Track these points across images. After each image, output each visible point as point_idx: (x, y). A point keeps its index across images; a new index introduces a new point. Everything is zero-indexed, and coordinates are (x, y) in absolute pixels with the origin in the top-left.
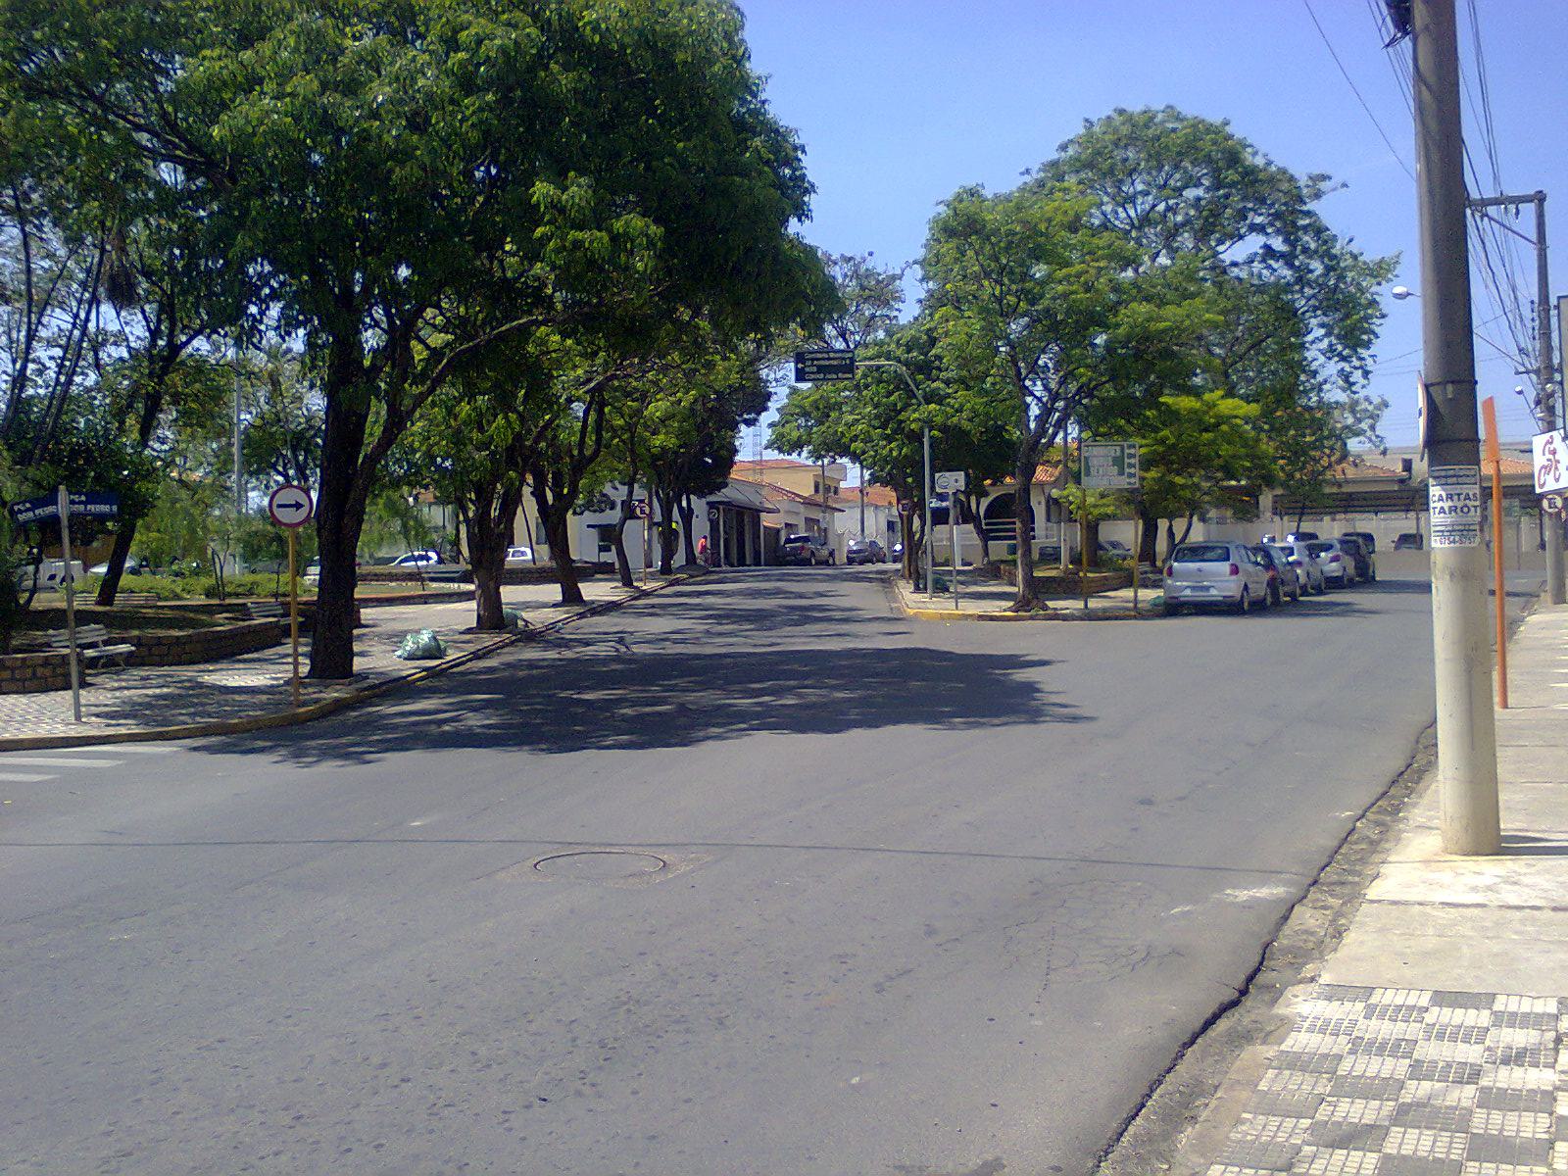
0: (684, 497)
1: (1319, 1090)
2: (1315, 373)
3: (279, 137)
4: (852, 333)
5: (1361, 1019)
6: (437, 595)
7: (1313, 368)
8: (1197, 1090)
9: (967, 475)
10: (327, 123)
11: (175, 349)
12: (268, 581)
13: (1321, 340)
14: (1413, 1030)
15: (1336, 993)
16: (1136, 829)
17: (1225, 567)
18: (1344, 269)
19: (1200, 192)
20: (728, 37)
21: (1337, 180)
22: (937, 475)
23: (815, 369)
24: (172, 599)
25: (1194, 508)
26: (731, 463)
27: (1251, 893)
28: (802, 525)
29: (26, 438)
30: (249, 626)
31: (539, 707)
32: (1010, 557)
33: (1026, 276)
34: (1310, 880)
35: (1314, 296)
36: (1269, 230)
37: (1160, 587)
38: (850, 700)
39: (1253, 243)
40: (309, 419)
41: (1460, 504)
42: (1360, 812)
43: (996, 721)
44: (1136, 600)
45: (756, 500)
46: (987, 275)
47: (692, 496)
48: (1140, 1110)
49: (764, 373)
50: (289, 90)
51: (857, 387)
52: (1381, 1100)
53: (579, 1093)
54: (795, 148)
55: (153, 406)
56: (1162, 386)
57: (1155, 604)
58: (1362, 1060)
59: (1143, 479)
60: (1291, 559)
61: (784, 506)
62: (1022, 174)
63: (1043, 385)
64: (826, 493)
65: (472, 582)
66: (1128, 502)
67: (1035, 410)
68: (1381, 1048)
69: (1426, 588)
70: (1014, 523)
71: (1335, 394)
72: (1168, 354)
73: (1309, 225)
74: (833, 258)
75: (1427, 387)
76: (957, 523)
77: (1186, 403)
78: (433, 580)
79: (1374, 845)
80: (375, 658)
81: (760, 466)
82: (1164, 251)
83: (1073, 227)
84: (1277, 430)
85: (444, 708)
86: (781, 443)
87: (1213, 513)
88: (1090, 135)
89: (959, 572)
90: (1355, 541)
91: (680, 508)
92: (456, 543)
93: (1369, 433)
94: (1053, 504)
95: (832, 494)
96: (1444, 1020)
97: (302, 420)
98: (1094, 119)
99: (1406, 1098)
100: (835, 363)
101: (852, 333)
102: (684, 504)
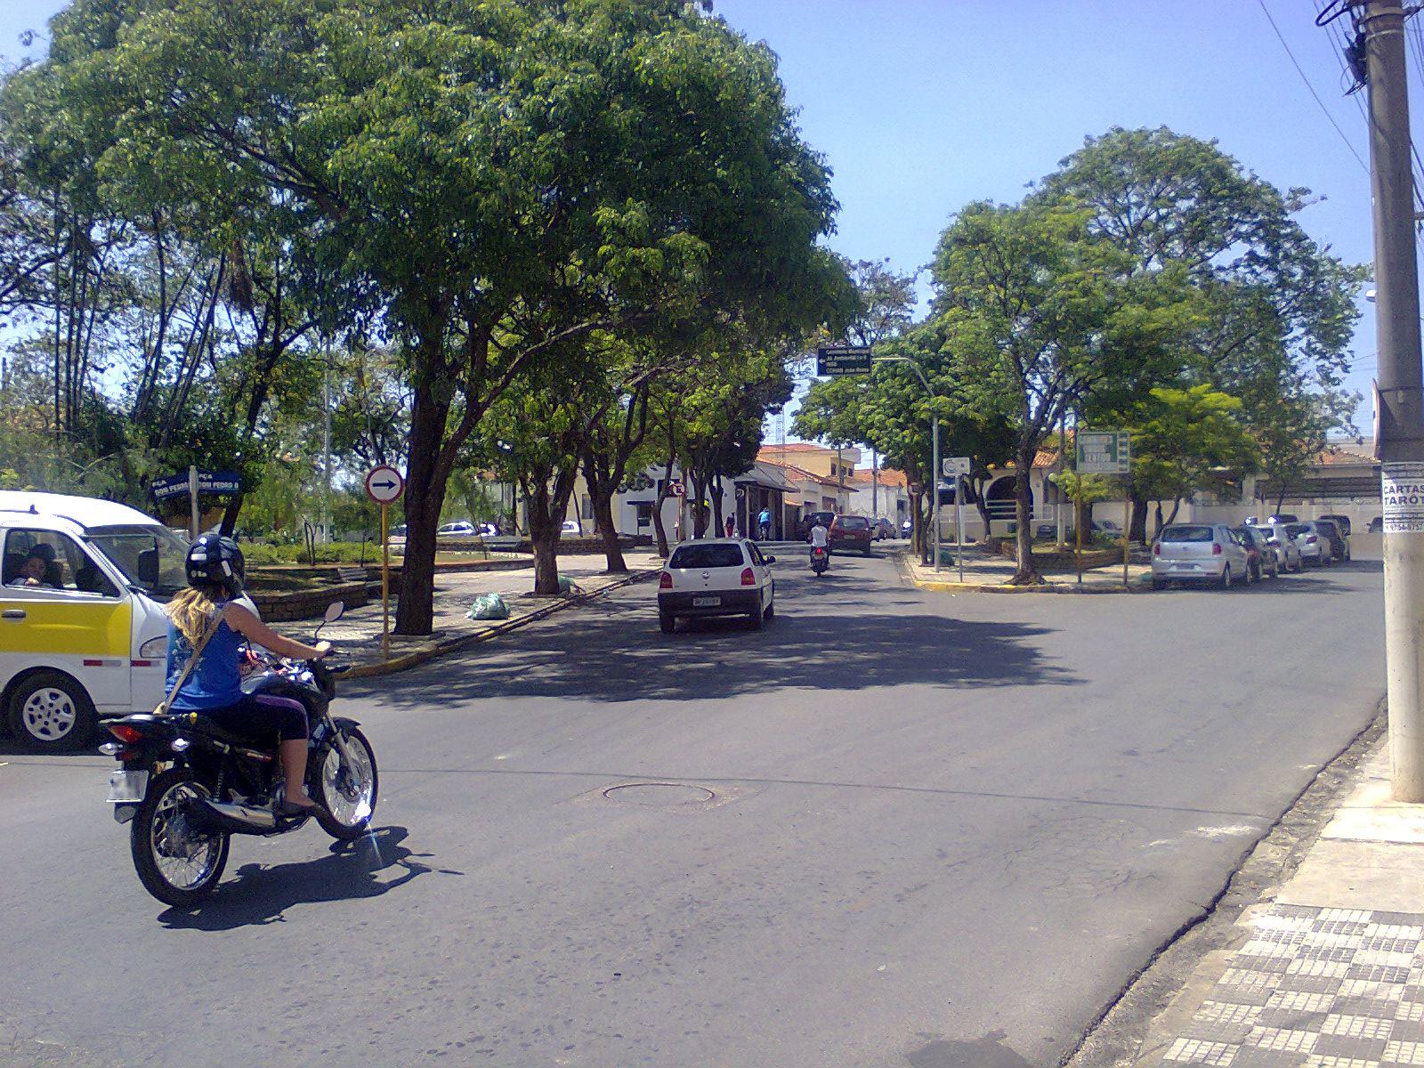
0: (715, 478)
1: (1270, 985)
2: (1294, 369)
3: (385, 171)
4: (869, 331)
5: (1309, 931)
6: (499, 563)
7: (1293, 364)
8: (1170, 984)
9: (972, 461)
10: (427, 160)
11: (278, 346)
12: (353, 548)
13: (1300, 339)
14: (1354, 941)
15: (1288, 911)
16: (1120, 776)
17: (1208, 547)
18: (1322, 273)
19: (1191, 203)
20: (764, 78)
21: (1316, 194)
22: (945, 460)
23: (835, 364)
24: (269, 564)
25: (1180, 491)
26: (758, 447)
27: (1220, 831)
28: (819, 502)
29: (154, 423)
30: (340, 589)
31: (598, 662)
32: (1010, 535)
33: (1028, 281)
34: (1273, 822)
35: (1295, 297)
36: (1254, 239)
37: (1149, 564)
38: (869, 661)
39: (1239, 250)
40: (386, 406)
41: (1409, 496)
42: (1321, 765)
43: (997, 682)
44: (1126, 576)
45: (778, 481)
46: (993, 278)
47: (722, 477)
48: (1119, 998)
49: (788, 367)
50: (392, 130)
51: (873, 381)
52: (1323, 993)
53: (656, 971)
54: (824, 170)
55: (260, 395)
56: (1152, 380)
57: (1144, 578)
58: (1308, 963)
59: (1134, 465)
60: (1270, 540)
61: (804, 487)
62: (1026, 186)
63: (1042, 378)
64: (843, 471)
65: (531, 552)
66: (1120, 485)
67: (1035, 403)
68: (1328, 955)
69: (1378, 566)
70: (1015, 504)
71: (1313, 388)
72: (1156, 352)
73: (1291, 233)
74: (853, 263)
75: (1380, 393)
76: (962, 503)
77: (1173, 396)
78: (493, 550)
79: (1332, 793)
80: (451, 618)
81: (782, 449)
82: (1156, 256)
83: (1073, 235)
84: (1261, 421)
85: (519, 662)
86: (805, 430)
87: (1199, 496)
88: (1089, 151)
89: (965, 548)
90: (1331, 524)
91: (712, 487)
92: (513, 517)
93: (1345, 423)
94: (1050, 487)
95: (847, 475)
96: (1380, 934)
97: (380, 407)
98: (1095, 137)
99: (1344, 992)
100: (854, 358)
101: (869, 331)
102: (715, 483)
